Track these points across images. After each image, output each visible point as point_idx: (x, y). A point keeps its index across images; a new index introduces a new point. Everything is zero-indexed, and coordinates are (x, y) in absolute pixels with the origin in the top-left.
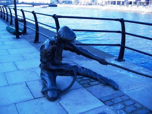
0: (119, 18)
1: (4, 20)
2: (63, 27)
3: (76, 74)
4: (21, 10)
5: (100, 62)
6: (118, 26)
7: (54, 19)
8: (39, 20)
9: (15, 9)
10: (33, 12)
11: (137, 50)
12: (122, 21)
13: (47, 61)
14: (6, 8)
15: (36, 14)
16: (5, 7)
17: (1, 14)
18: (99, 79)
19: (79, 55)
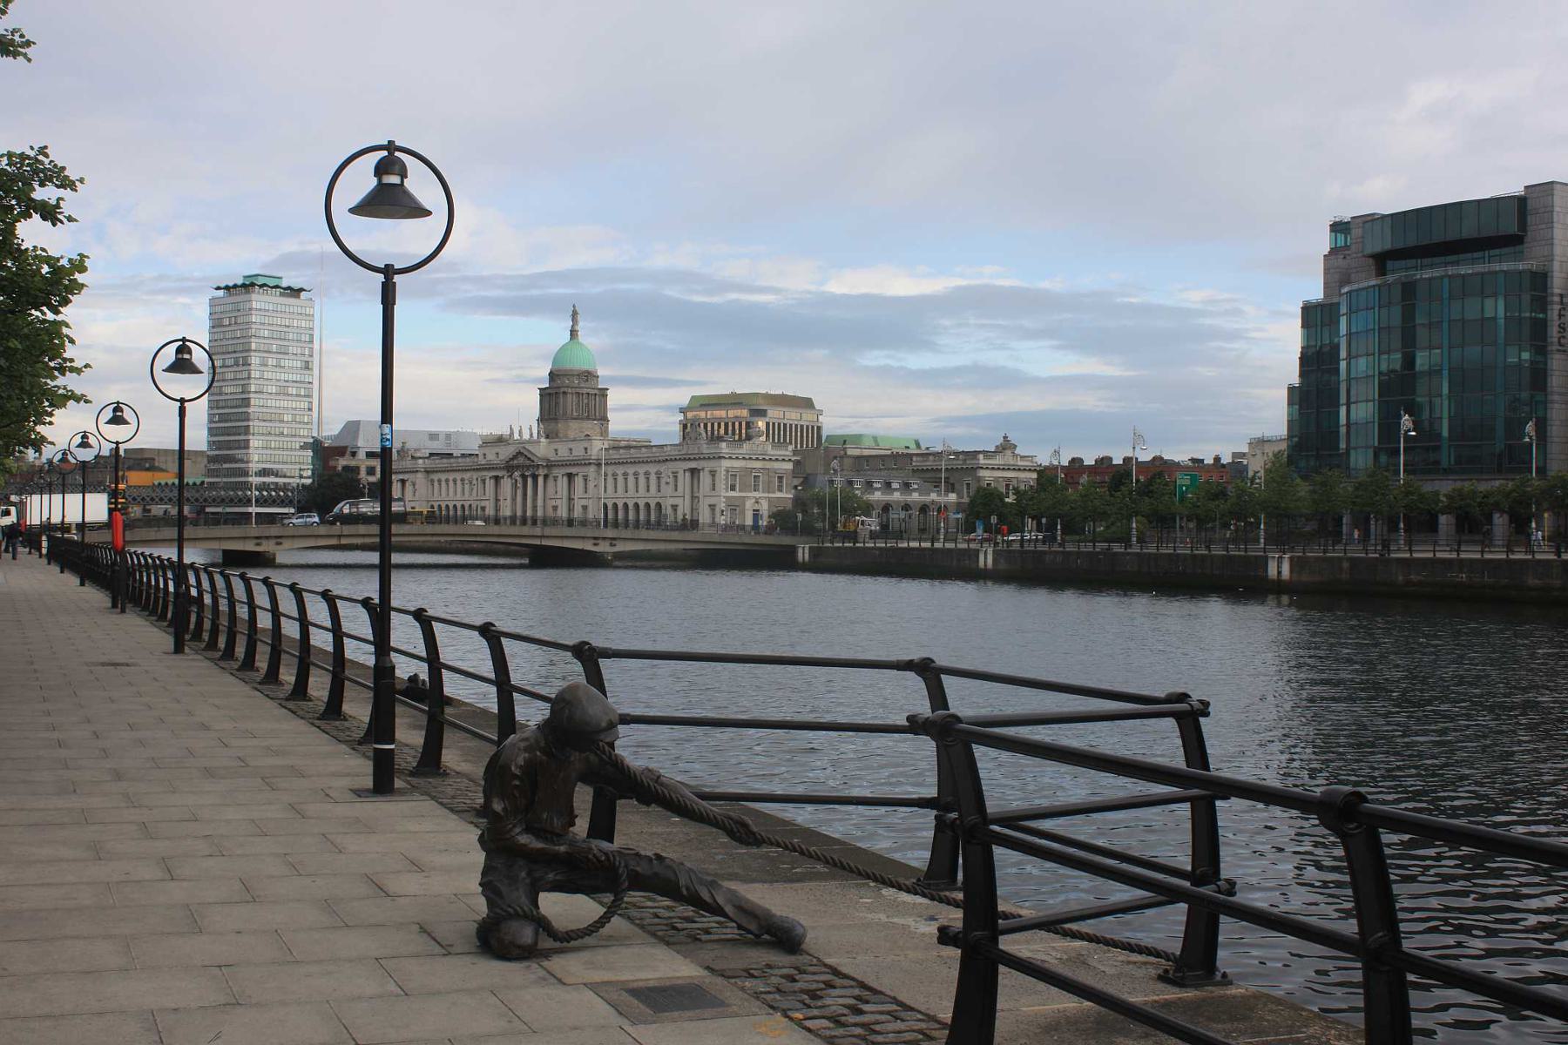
0: (916, 655)
1: (210, 654)
2: (768, 910)
3: (627, 884)
4: (293, 588)
5: (730, 833)
6: (912, 697)
7: (920, 678)
8: (446, 656)
9: (380, 614)
10: (488, 632)
11: (713, 719)
12: (927, 670)
13: (505, 809)
14: (247, 581)
15: (304, 594)
16: (222, 573)
17: (193, 618)
18: (728, 909)
19: (648, 804)
